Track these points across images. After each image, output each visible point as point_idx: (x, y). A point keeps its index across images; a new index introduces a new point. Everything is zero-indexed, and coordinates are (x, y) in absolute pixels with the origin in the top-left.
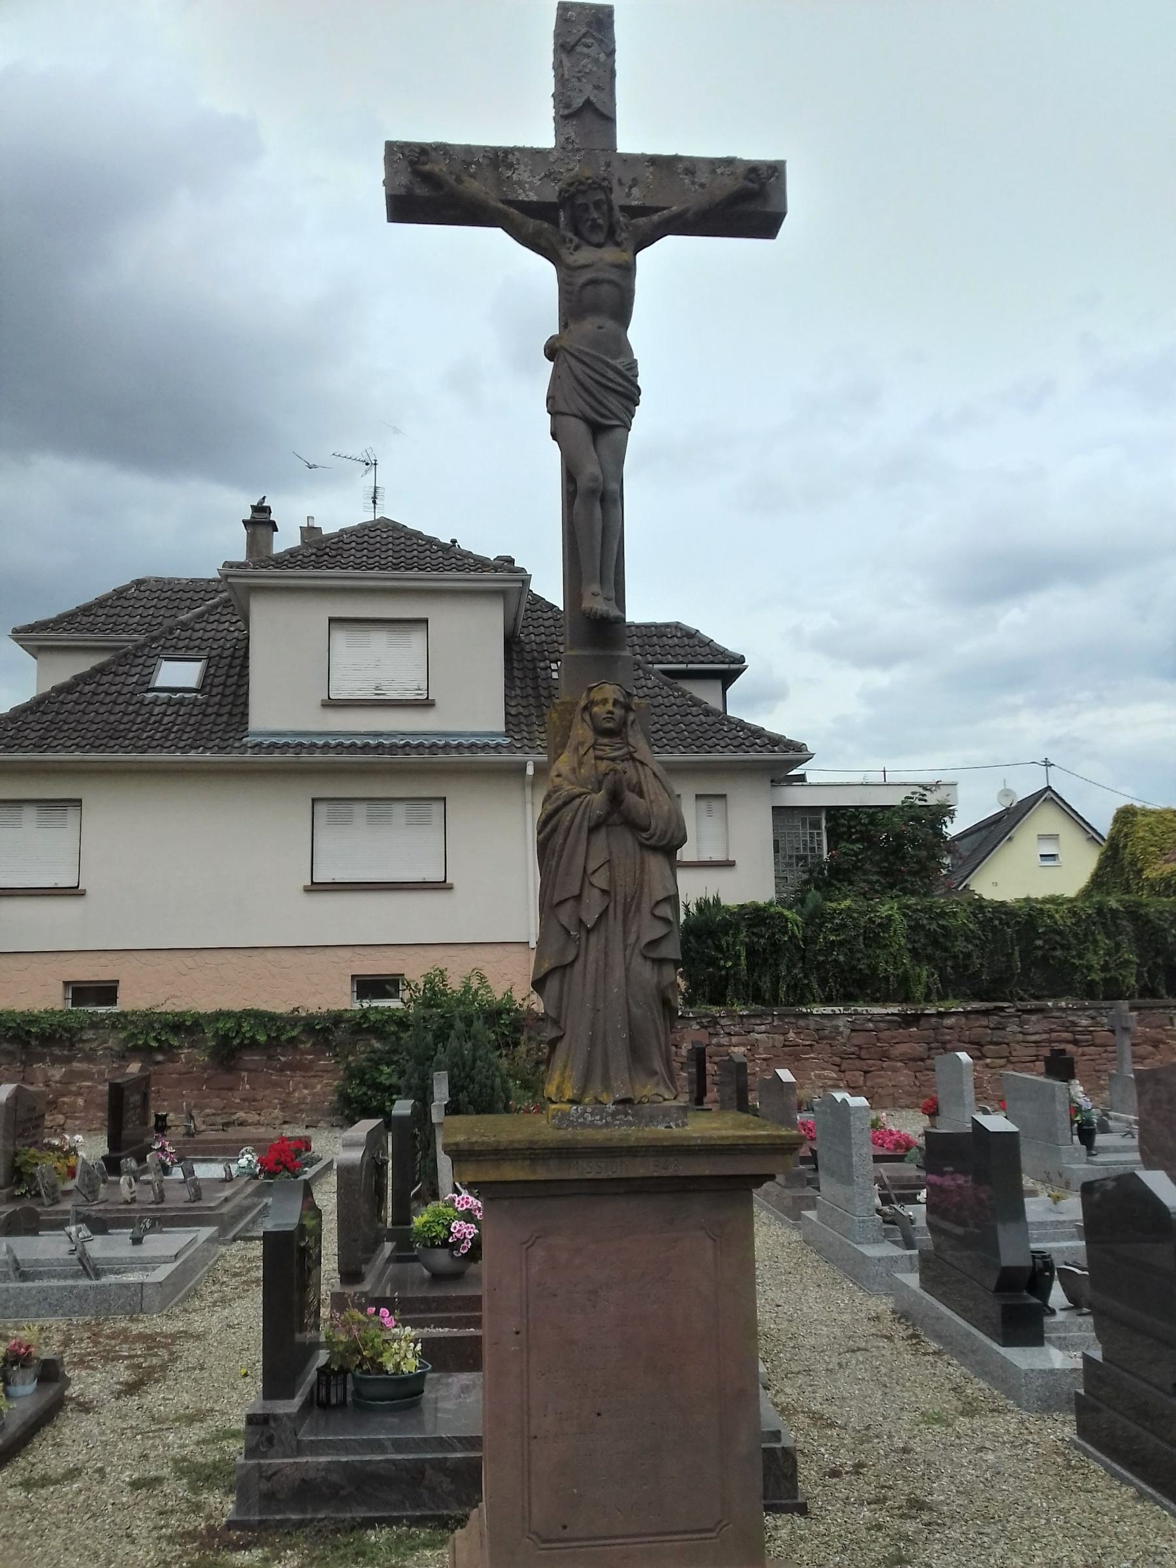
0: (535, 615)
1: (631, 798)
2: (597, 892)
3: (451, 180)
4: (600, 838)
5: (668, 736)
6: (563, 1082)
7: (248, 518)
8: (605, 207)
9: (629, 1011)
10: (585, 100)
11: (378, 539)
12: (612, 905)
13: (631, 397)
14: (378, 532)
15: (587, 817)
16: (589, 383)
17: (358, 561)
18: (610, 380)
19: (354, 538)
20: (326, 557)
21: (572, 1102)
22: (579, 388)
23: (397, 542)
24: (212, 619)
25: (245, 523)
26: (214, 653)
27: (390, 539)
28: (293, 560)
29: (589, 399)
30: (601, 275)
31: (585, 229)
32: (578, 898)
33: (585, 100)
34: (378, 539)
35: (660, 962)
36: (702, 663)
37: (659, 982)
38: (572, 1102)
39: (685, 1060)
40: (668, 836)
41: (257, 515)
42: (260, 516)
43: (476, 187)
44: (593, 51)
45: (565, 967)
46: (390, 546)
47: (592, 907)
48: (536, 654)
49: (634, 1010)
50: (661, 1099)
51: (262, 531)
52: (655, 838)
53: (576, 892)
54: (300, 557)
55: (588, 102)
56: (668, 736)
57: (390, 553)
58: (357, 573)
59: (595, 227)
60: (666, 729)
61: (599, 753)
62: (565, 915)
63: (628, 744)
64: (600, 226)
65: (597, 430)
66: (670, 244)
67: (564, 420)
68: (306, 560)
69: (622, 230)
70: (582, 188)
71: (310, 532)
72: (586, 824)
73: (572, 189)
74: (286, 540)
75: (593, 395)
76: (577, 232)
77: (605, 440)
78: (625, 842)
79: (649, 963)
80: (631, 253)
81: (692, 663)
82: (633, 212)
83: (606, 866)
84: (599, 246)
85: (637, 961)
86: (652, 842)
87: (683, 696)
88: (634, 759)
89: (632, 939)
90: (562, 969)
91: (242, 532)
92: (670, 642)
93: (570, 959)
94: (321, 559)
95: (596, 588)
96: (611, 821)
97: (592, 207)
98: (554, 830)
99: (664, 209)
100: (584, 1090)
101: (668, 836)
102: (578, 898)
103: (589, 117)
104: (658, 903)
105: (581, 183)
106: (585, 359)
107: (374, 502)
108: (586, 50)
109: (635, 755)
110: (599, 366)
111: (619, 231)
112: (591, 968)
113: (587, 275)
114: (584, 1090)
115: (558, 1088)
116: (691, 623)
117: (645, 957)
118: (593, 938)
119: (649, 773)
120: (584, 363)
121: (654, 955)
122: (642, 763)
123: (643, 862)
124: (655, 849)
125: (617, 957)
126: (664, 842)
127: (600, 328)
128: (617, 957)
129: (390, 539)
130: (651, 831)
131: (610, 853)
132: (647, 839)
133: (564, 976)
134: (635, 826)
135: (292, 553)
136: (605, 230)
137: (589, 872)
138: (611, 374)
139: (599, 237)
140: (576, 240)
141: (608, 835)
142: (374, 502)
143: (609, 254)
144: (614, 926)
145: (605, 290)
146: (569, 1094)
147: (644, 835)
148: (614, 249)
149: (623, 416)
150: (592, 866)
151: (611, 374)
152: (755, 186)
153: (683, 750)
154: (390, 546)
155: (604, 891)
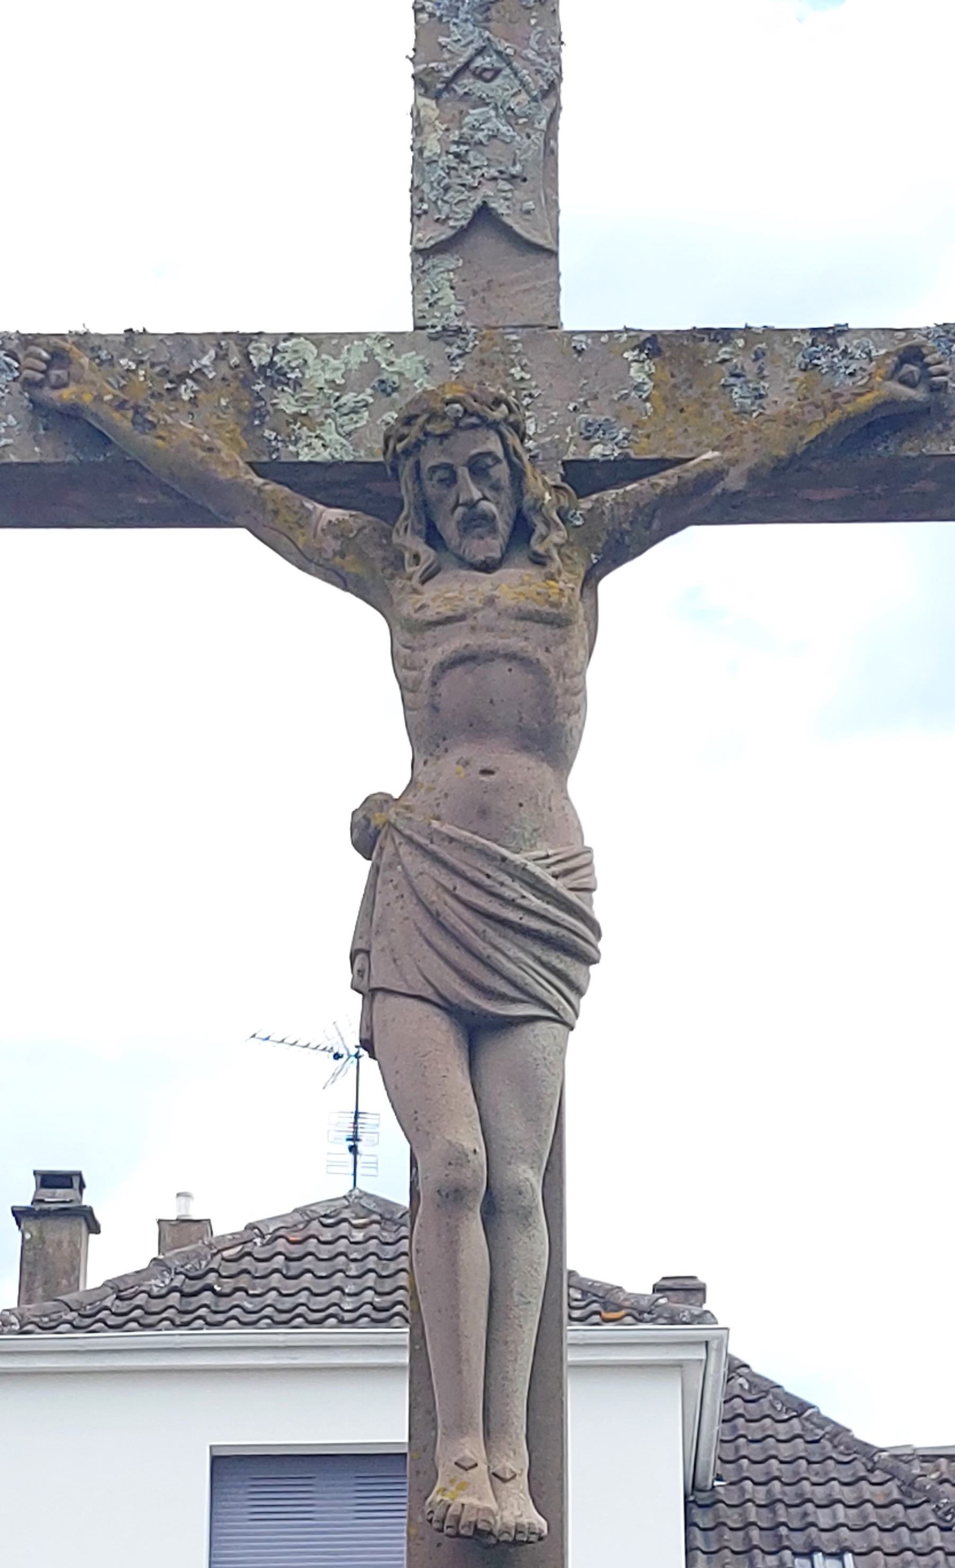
0: (754, 1430)
3: (123, 421)
7: (27, 1202)
8: (501, 472)
10: (484, 211)
11: (342, 1245)
13: (569, 943)
14: (344, 1228)
16: (453, 914)
17: (288, 1303)
18: (511, 903)
19: (281, 1245)
20: (207, 1297)
22: (427, 926)
23: (390, 1251)
25: (19, 1214)
27: (373, 1245)
28: (123, 1307)
29: (456, 955)
30: (489, 640)
31: (449, 529)
33: (484, 211)
34: (342, 1245)
41: (47, 1194)
43: (195, 433)
44: (500, 87)
46: (371, 1262)
48: (755, 1533)
51: (59, 1232)
54: (141, 1299)
55: (484, 213)
57: (371, 1279)
58: (281, 1335)
59: (476, 521)
64: (488, 519)
65: (478, 1031)
66: (697, 554)
67: (386, 1006)
68: (156, 1305)
69: (548, 523)
70: (435, 428)
71: (178, 1231)
73: (414, 432)
74: (118, 1251)
75: (473, 942)
76: (433, 537)
77: (500, 1054)
80: (569, 582)
82: (582, 477)
84: (488, 567)
94: (195, 1302)
95: (472, 1447)
97: (463, 472)
99: (662, 464)
103: (486, 244)
105: (433, 416)
106: (443, 853)
107: (353, 1149)
108: (479, 88)
110: (477, 868)
111: (541, 528)
113: (456, 641)
120: (444, 864)
127: (486, 772)
129: (373, 1245)
135: (119, 1288)
136: (503, 526)
138: (514, 889)
139: (493, 547)
140: (427, 554)
142: (353, 1149)
143: (514, 584)
145: (500, 675)
148: (532, 572)
149: (554, 998)
151: (514, 889)
152: (919, 394)
154: (371, 1262)
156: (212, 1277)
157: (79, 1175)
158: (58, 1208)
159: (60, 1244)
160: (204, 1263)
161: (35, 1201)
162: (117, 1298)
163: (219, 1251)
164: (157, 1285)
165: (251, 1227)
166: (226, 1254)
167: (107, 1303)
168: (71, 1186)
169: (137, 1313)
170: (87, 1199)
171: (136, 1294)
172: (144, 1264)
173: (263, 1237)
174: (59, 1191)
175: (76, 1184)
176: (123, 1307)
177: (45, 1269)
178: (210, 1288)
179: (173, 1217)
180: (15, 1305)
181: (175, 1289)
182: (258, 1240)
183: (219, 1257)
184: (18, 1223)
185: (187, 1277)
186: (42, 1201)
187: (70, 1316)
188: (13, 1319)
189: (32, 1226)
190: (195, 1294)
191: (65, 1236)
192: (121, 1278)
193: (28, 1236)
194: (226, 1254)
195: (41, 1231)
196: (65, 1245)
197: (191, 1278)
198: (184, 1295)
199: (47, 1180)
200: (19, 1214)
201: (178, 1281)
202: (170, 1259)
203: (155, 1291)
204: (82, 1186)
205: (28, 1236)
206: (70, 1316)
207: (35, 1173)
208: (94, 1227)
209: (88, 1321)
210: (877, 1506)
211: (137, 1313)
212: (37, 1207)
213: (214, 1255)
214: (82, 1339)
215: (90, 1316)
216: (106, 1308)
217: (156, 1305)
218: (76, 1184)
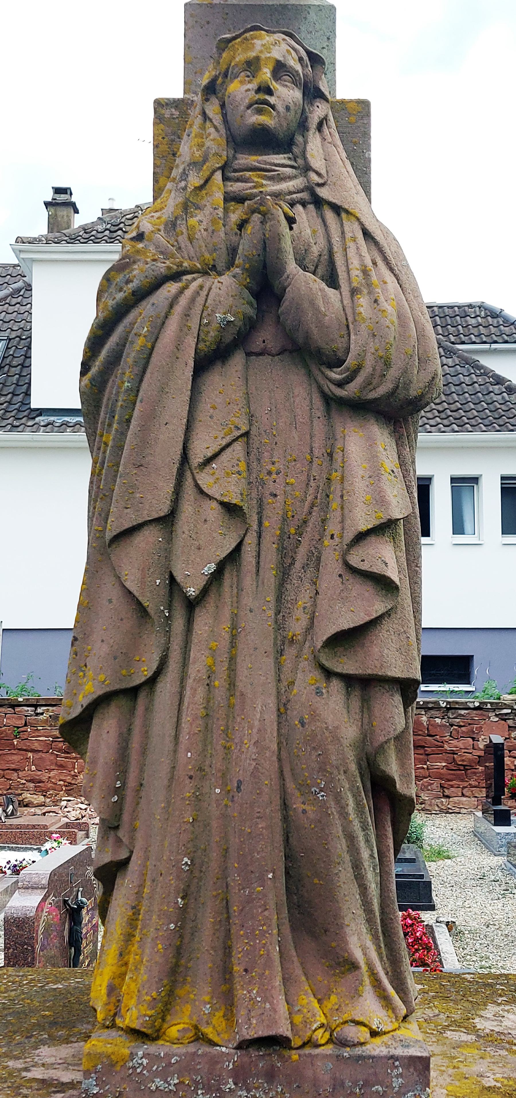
1: (303, 283)
2: (212, 511)
4: (225, 384)
5: (470, 415)
6: (122, 976)
7: (50, 200)
9: (285, 806)
12: (251, 539)
15: (194, 324)
20: (120, 233)
21: (137, 1034)
24: (14, 301)
25: (47, 204)
26: (13, 335)
28: (87, 236)
32: (167, 521)
35: (363, 685)
36: (506, 342)
37: (365, 737)
38: (137, 1034)
39: (482, 753)
40: (393, 373)
42: (62, 198)
45: (132, 693)
47: (199, 549)
49: (297, 805)
50: (363, 1034)
51: (63, 212)
52: (359, 379)
53: (163, 509)
56: (470, 415)
60: (466, 407)
61: (236, 187)
62: (134, 564)
63: (307, 169)
68: (100, 235)
72: (191, 342)
78: (286, 396)
79: (336, 684)
81: (496, 342)
83: (238, 447)
85: (306, 679)
86: (351, 390)
87: (485, 374)
88: (318, 202)
89: (297, 626)
90: (129, 695)
91: (44, 214)
92: (473, 321)
93: (146, 671)
94: (115, 234)
96: (257, 343)
98: (115, 359)
100: (166, 1006)
101: (393, 373)
102: (167, 521)
104: (361, 537)
109: (323, 193)
112: (195, 697)
114: (166, 1006)
115: (112, 989)
116: (495, 303)
117: (328, 674)
118: (203, 622)
119: (352, 229)
121: (348, 665)
122: (337, 209)
123: (331, 437)
124: (360, 408)
125: (256, 672)
126: (382, 390)
128: (256, 672)
130: (350, 361)
131: (251, 417)
132: (340, 384)
133: (132, 711)
134: (309, 353)
135: (85, 229)
137: (197, 457)
141: (247, 367)
144: (253, 595)
146: (133, 1016)
147: (335, 375)
150: (201, 448)
153: (484, 428)
155: (230, 509)
156: (122, 225)
157: (70, 189)
158: (61, 202)
159: (63, 217)
160: (119, 220)
161: (53, 199)
162: (85, 232)
163: (124, 216)
164: (100, 228)
165: (137, 206)
166: (128, 217)
167: (81, 234)
168: (66, 193)
169: (92, 238)
170: (73, 199)
171: (92, 231)
172: (95, 219)
173: (142, 210)
174: (62, 195)
175: (69, 193)
176: (87, 236)
177: (58, 226)
178: (121, 229)
179: (108, 208)
180: (46, 233)
181: (106, 230)
182: (140, 212)
183: (125, 218)
184: (47, 208)
185: (112, 225)
186: (55, 199)
187: (66, 238)
188: (43, 239)
189: (52, 210)
190: (116, 231)
191: (65, 213)
192: (86, 225)
193: (50, 213)
194: (128, 217)
195: (56, 211)
196: (65, 217)
197: (114, 226)
198: (111, 232)
199: (58, 191)
200: (47, 204)
201: (109, 226)
202: (105, 218)
203: (99, 230)
204: (71, 194)
205: (50, 213)
206: (66, 238)
207: (53, 188)
208: (76, 211)
209: (73, 241)
210: (449, 367)
211: (92, 238)
212: (54, 201)
213: (122, 217)
214: (71, 247)
215: (73, 239)
216: (80, 236)
217: (100, 235)
218: (69, 193)
